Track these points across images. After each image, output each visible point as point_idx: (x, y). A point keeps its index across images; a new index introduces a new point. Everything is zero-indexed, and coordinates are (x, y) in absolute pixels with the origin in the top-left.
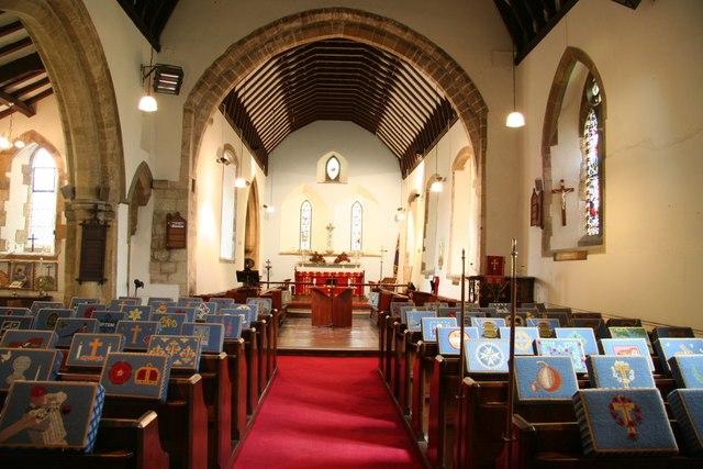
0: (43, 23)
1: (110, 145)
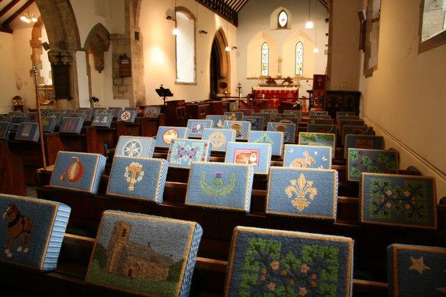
1: (64, 14)
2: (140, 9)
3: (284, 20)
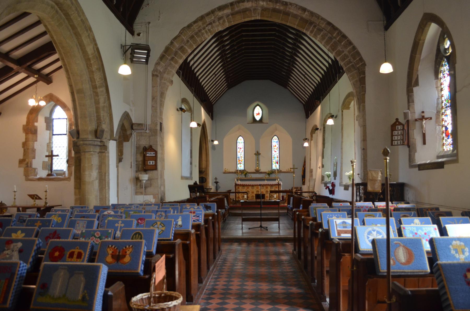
2: (165, 99)
3: (258, 114)
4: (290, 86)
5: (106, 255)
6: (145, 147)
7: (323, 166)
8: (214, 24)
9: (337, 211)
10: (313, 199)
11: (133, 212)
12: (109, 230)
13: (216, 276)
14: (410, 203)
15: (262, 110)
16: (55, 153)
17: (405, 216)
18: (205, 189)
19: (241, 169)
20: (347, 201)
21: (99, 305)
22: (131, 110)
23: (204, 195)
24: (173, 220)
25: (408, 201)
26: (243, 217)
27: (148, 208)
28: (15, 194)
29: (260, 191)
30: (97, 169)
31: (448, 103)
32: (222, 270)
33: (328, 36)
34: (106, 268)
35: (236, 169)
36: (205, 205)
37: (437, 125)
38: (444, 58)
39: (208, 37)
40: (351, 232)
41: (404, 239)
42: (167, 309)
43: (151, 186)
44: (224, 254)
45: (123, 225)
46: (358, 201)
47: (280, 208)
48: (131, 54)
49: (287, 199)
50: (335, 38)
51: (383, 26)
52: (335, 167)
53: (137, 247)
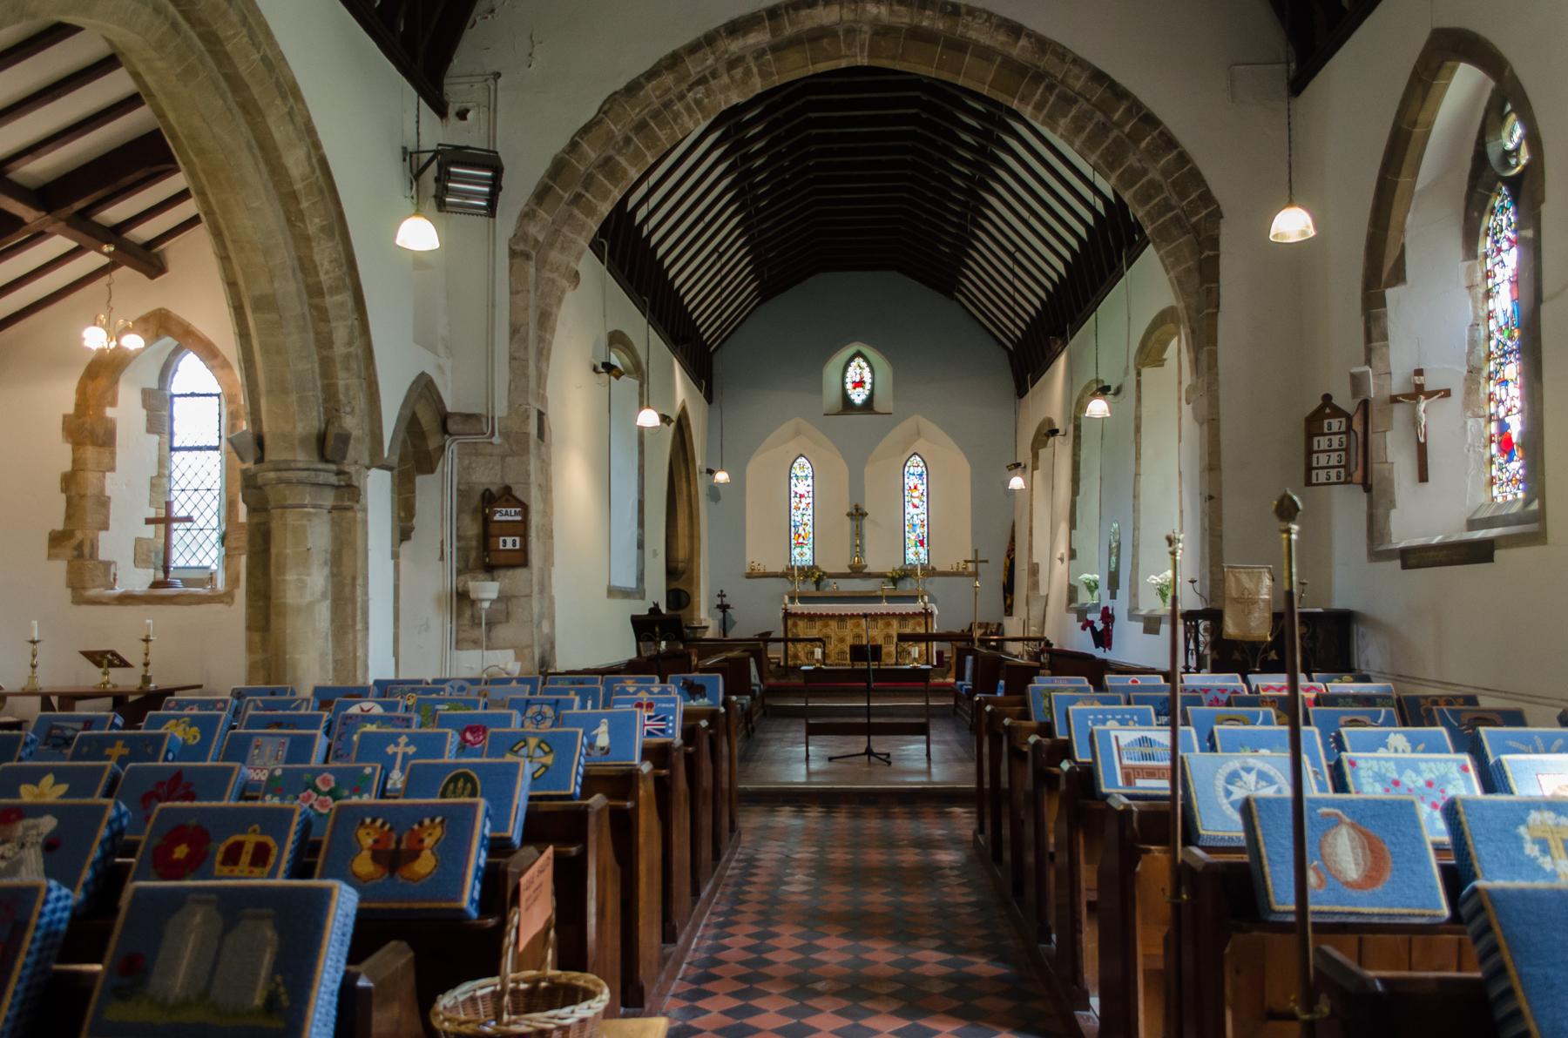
0: (160, 46)
1: (340, 333)
3: (859, 384)
4: (964, 290)
5: (354, 850)
6: (488, 490)
7: (1072, 554)
8: (712, 82)
9: (1120, 704)
10: (1042, 664)
11: (447, 707)
12: (364, 768)
13: (721, 919)
14: (1373, 679)
15: (872, 371)
16: (178, 511)
17: (1354, 723)
18: (688, 628)
19: (803, 563)
20: (1154, 669)
21: (325, 1025)
22: (440, 368)
23: (681, 647)
24: (581, 731)
25: (1364, 673)
26: (811, 721)
27: (497, 692)
28: (34, 650)
29: (864, 635)
30: (326, 563)
31: (1511, 338)
32: (741, 897)
33: (1095, 121)
34: (352, 897)
35: (788, 563)
36: (686, 681)
37: (1469, 414)
38: (1499, 184)
39: (696, 126)
40: (1168, 773)
41: (1352, 801)
42: (556, 1033)
43: (507, 621)
44: (746, 845)
45: (411, 750)
46: (1191, 670)
47: (931, 691)
48: (437, 180)
49: (953, 660)
50: (1119, 125)
51: (1286, 81)
52: (1114, 559)
53: (459, 821)
